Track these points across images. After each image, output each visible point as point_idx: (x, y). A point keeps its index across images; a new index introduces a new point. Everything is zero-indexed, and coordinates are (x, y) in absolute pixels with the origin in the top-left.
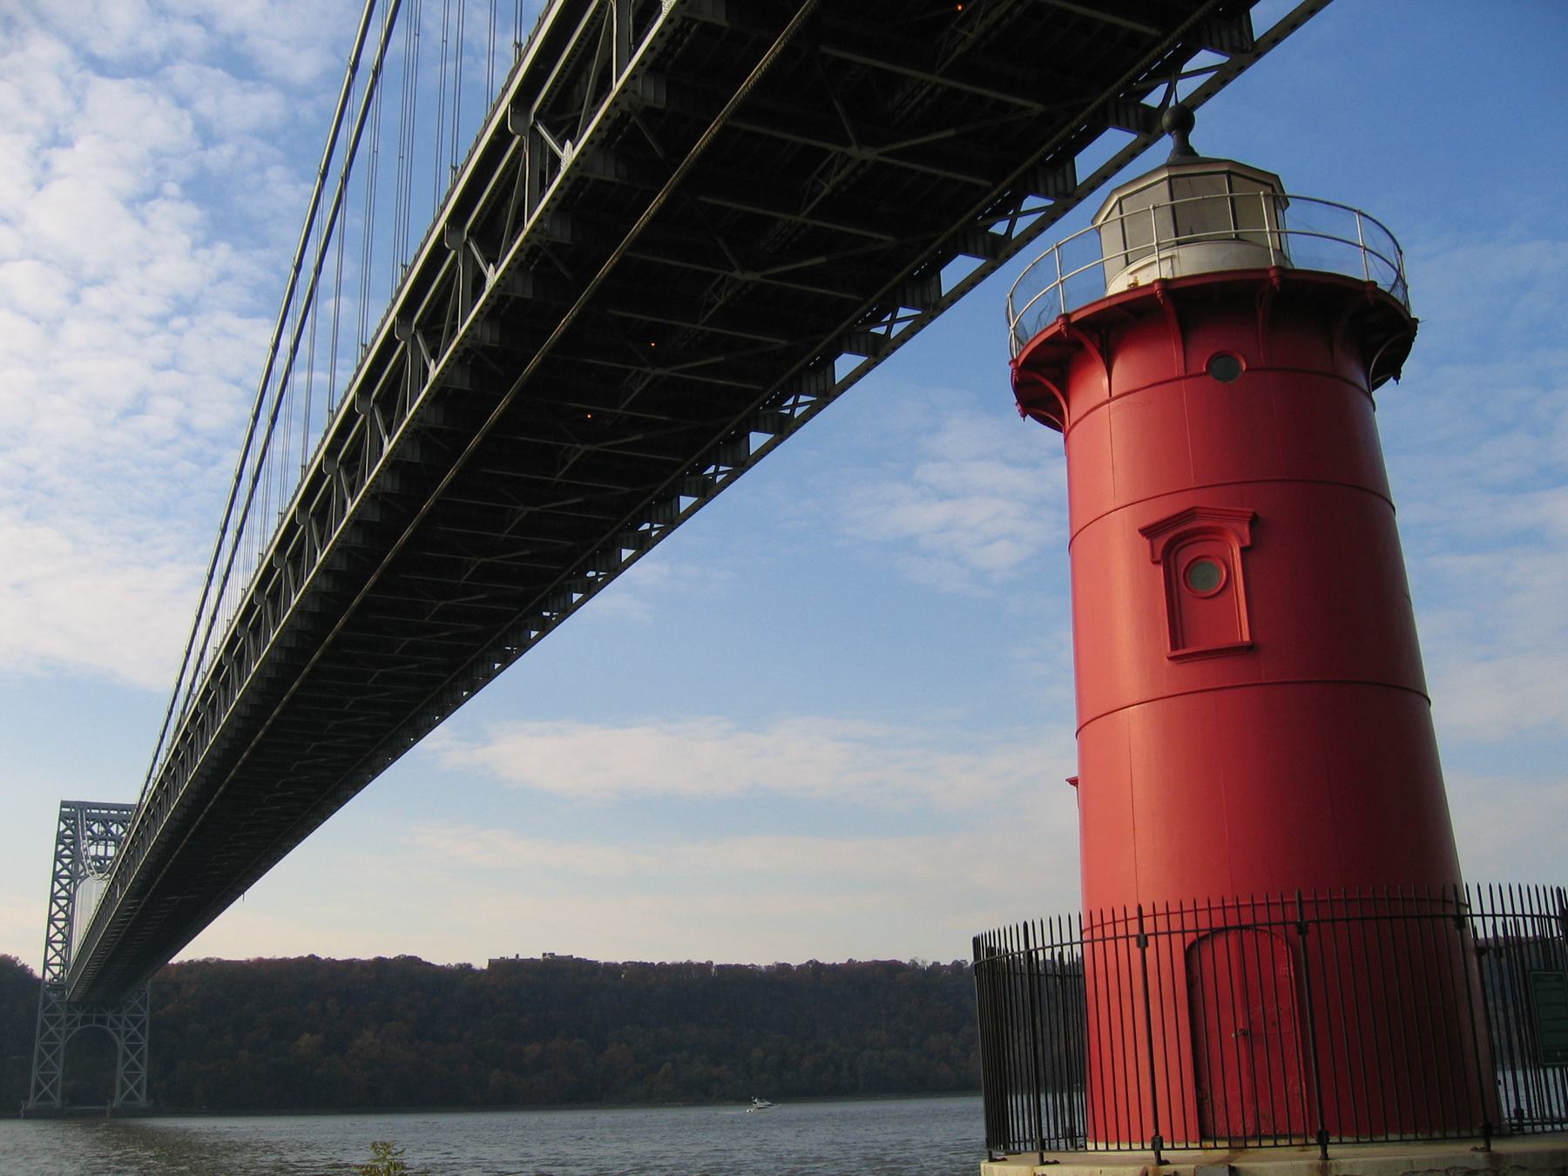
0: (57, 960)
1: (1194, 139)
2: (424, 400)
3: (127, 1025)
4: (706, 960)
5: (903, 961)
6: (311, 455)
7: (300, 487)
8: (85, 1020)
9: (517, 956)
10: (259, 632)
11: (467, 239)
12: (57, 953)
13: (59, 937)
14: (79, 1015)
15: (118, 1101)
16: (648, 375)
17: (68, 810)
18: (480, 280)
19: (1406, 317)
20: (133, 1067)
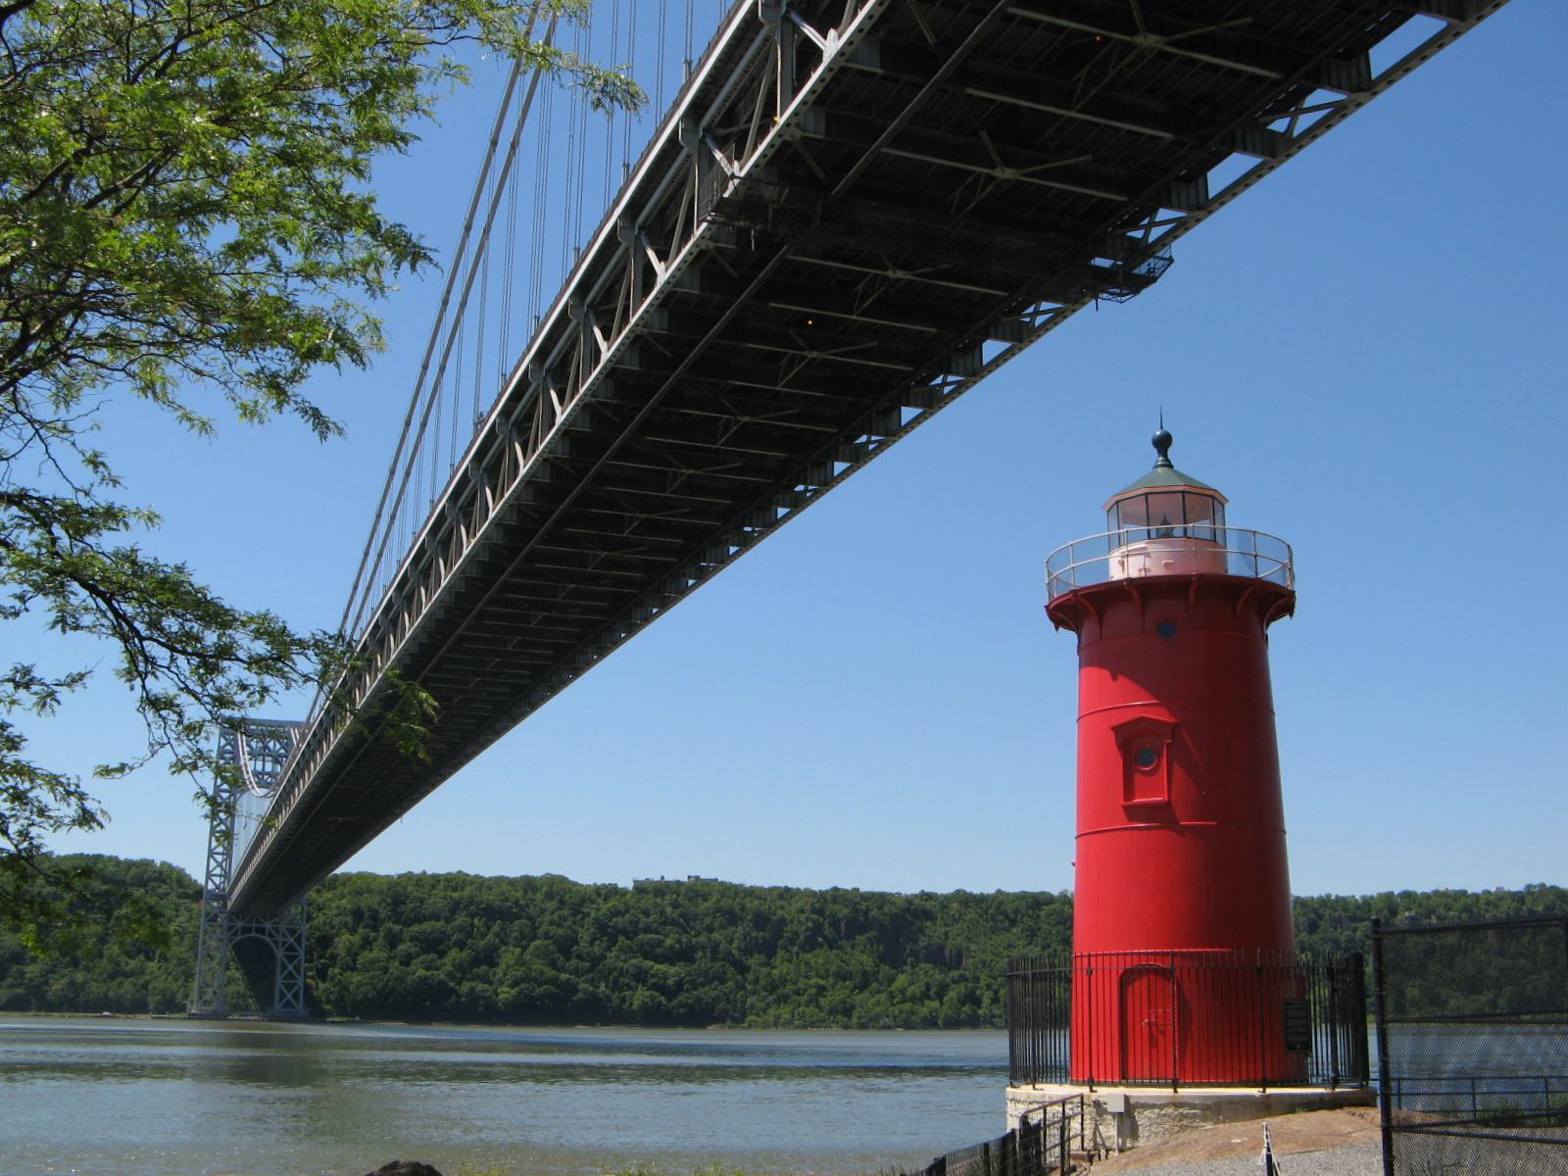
0: (218, 871)
2: (596, 378)
3: (284, 935)
8: (246, 930)
9: (662, 878)
10: (767, 98)
11: (704, 136)
12: (219, 865)
13: (220, 849)
14: (240, 924)
16: (805, 357)
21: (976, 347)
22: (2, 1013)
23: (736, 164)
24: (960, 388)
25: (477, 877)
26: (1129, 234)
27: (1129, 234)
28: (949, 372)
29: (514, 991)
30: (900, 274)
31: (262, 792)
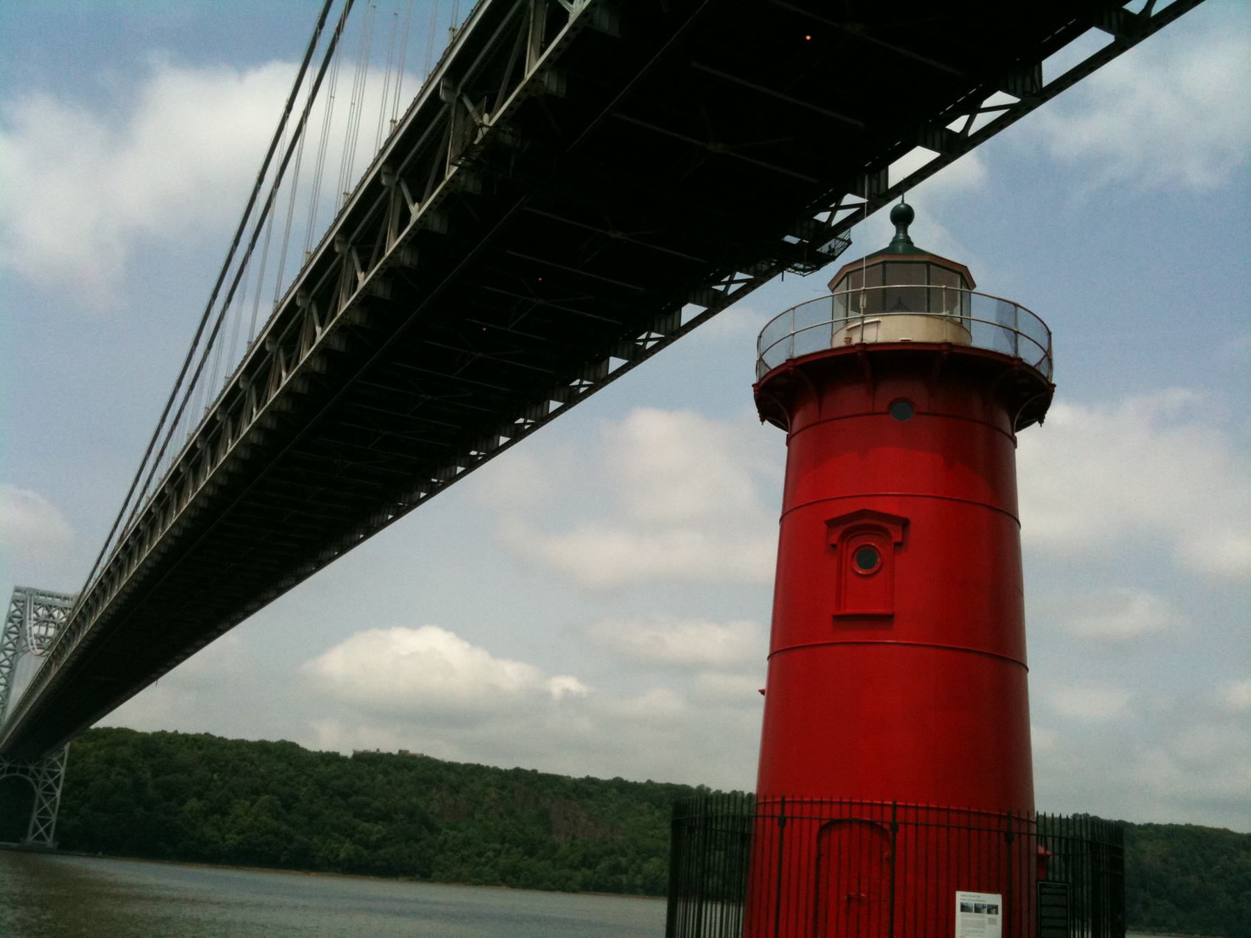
1: (912, 230)
3: (45, 778)
4: (732, 790)
5: (691, 786)
6: (257, 334)
7: (246, 357)
8: (10, 770)
11: (399, 180)
15: (30, 839)
17: (20, 594)
18: (406, 215)
19: (1045, 384)
20: (43, 822)
21: (678, 308)
22: (1241, 825)
23: (486, 117)
24: (662, 344)
25: (221, 739)
26: (714, 287)
27: (714, 287)
28: (652, 330)
29: (239, 838)
30: (619, 235)
31: (40, 651)
